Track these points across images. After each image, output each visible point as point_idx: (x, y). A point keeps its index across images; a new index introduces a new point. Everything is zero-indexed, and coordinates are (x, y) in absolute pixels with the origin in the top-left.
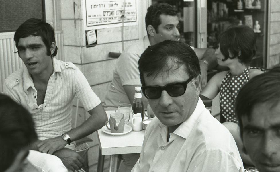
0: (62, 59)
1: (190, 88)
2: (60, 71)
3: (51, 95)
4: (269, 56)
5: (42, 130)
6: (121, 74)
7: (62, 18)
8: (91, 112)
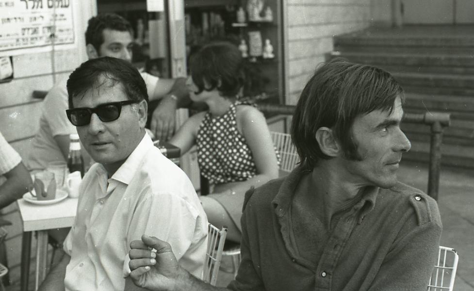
1: (127, 113)
6: (51, 120)
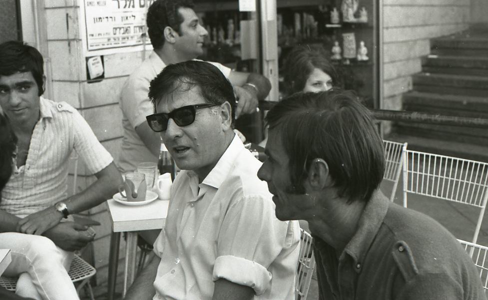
0: (50, 98)
2: (51, 116)
3: (37, 152)
4: (384, 98)
5: (23, 206)
7: (49, 38)
8: (100, 175)
